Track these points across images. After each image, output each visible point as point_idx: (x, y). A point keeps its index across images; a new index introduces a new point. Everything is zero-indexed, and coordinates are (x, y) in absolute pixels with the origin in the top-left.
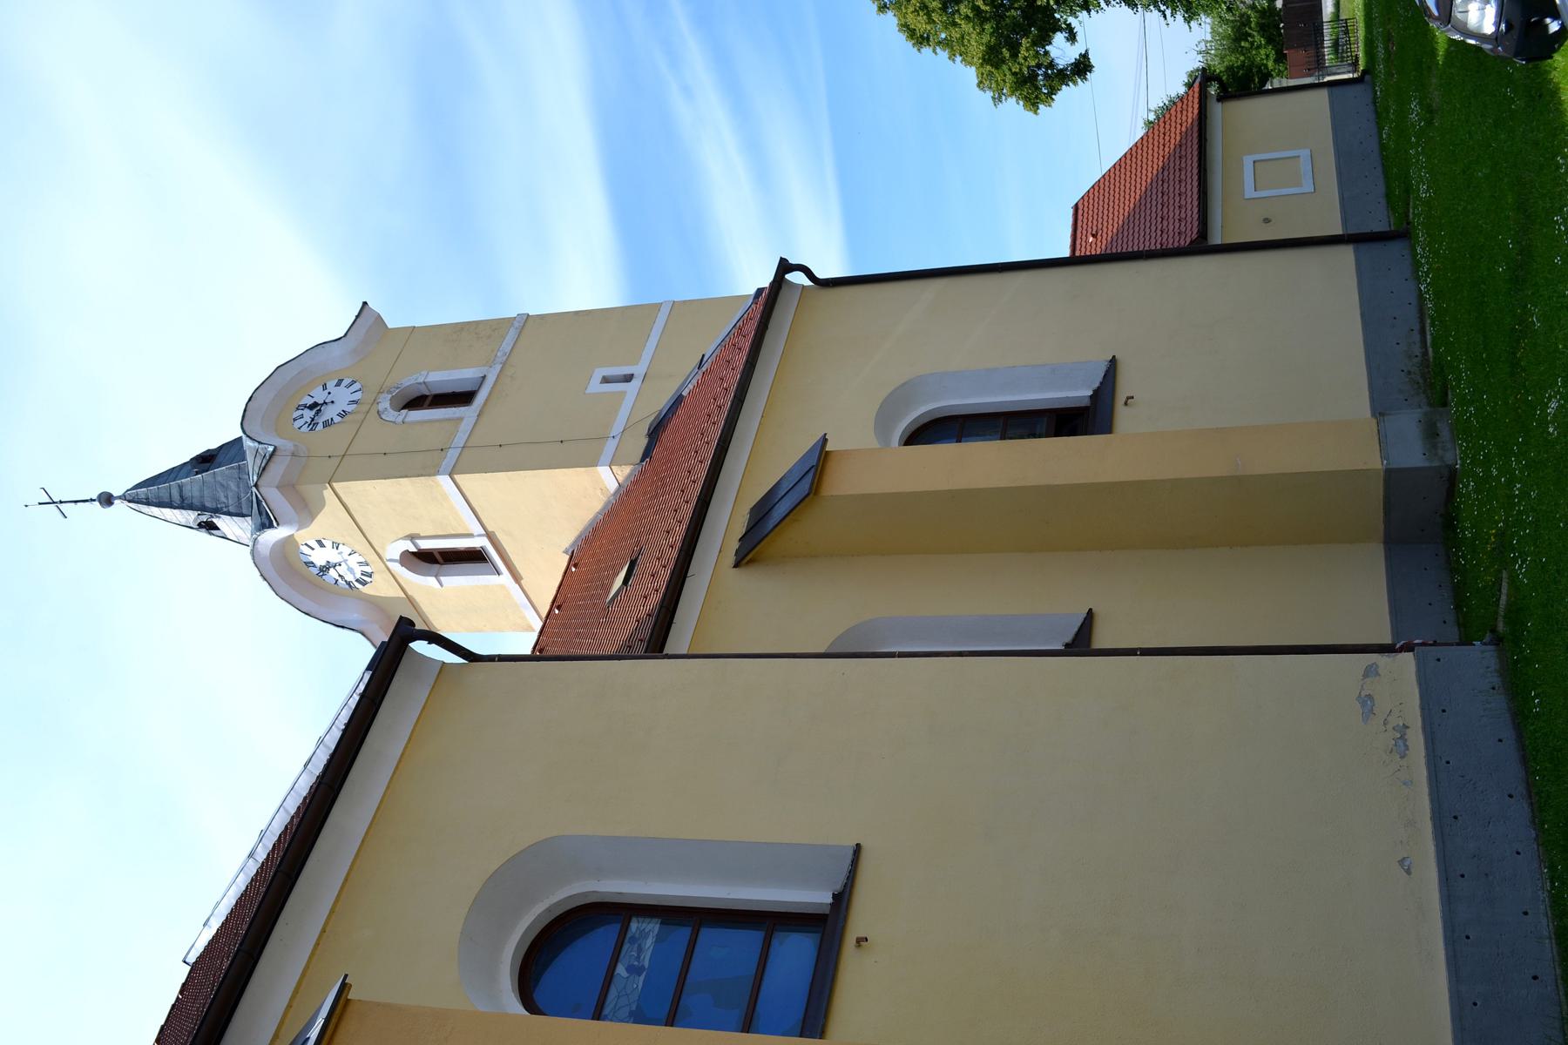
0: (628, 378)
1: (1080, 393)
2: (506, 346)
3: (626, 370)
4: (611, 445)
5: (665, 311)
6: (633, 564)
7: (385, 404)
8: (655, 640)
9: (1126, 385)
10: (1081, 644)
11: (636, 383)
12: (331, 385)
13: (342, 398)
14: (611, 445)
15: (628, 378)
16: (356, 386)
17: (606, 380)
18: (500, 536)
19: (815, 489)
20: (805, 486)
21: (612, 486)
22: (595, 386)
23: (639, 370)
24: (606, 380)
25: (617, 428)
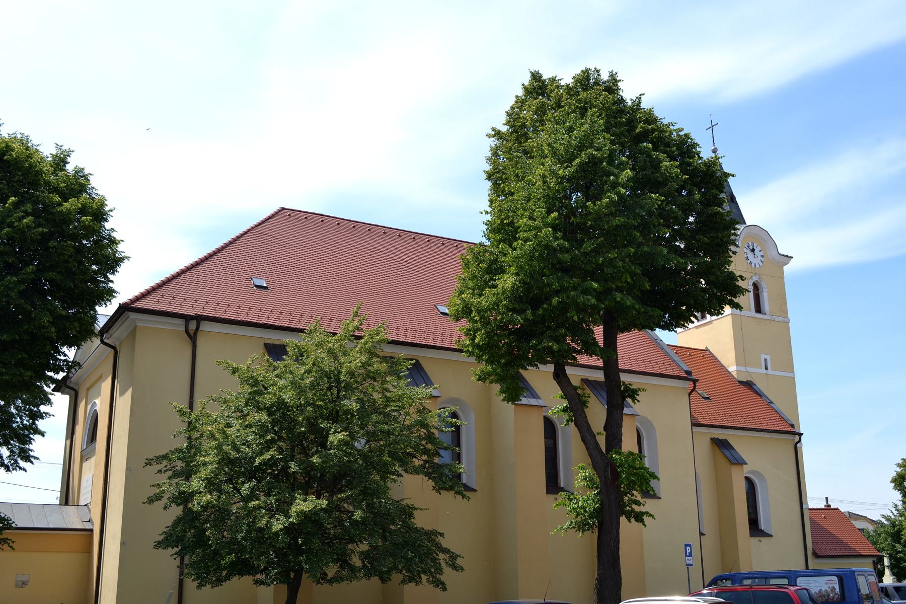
0: (766, 369)
1: (763, 526)
2: (778, 319)
3: (769, 367)
4: (743, 369)
5: (790, 375)
6: (708, 398)
7: (755, 279)
8: (695, 424)
9: (765, 540)
10: (701, 534)
11: (764, 371)
12: (762, 253)
13: (756, 261)
14: (743, 369)
15: (766, 369)
16: (761, 264)
17: (765, 360)
18: (710, 326)
19: (733, 464)
20: (734, 461)
21: (730, 369)
22: (763, 357)
23: (770, 371)
24: (765, 360)
25: (749, 369)
